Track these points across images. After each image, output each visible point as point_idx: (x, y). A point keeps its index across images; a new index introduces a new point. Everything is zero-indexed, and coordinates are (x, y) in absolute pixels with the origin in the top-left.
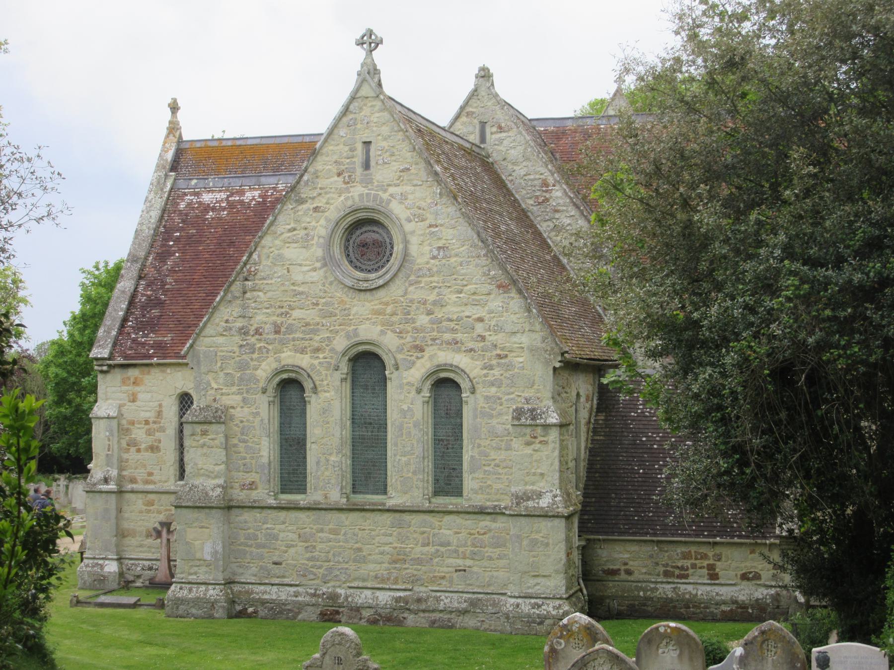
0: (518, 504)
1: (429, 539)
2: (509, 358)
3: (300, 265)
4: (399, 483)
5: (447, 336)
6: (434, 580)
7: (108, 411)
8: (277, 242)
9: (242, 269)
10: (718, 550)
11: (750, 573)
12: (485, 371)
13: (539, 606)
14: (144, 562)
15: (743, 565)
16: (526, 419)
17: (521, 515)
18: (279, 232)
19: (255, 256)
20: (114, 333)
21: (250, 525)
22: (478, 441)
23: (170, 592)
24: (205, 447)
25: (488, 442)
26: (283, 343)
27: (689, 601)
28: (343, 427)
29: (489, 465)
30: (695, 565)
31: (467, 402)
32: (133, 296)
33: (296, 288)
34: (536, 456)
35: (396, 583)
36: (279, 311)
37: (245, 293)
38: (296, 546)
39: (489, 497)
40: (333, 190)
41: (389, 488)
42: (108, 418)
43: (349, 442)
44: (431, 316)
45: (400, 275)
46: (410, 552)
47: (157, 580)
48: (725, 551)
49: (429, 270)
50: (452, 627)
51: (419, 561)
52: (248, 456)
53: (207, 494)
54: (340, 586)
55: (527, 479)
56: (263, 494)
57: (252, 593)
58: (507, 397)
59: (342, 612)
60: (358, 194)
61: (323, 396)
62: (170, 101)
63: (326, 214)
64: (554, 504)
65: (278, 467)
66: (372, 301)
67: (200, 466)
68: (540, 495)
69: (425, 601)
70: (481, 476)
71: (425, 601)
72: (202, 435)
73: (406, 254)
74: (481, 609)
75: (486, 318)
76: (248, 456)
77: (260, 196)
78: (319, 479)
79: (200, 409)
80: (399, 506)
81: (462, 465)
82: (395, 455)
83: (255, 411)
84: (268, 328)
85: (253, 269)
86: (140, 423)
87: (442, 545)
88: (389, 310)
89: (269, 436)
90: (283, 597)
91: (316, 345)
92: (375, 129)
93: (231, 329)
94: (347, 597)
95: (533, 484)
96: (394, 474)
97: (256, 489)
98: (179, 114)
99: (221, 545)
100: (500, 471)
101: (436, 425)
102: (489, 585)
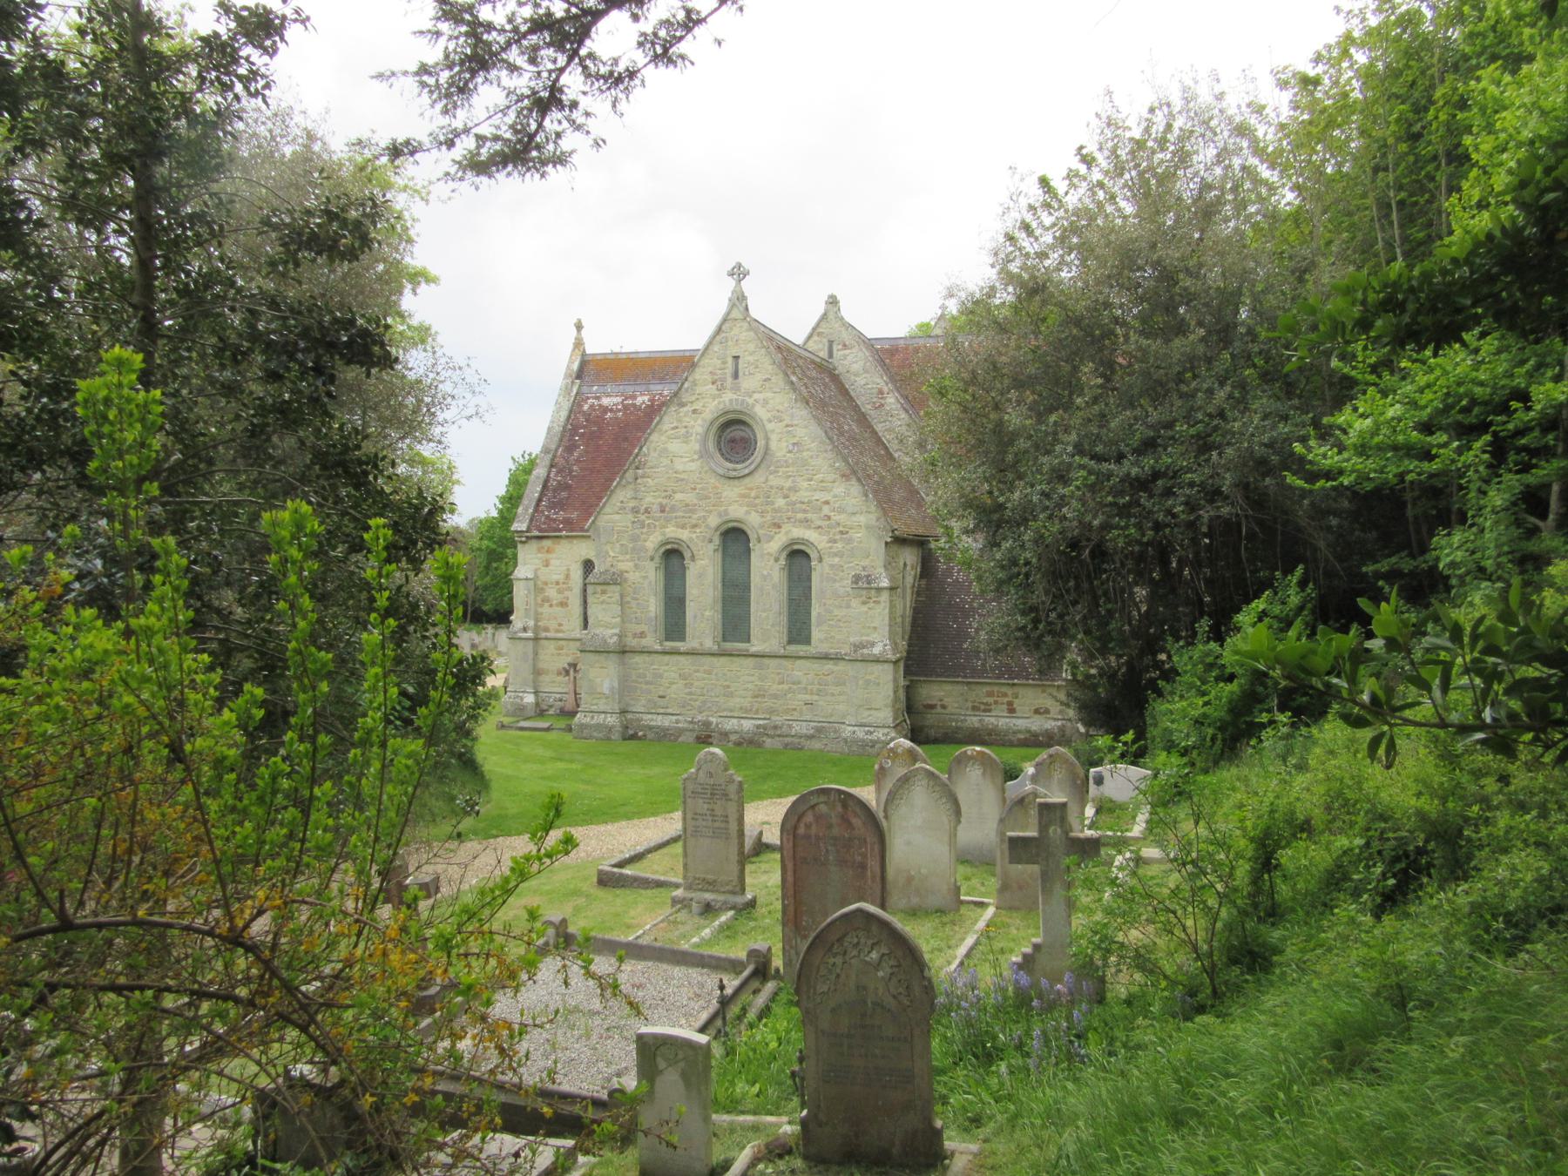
5: (800, 516)
6: (787, 711)
10: (1016, 689)
26: (668, 520)
28: (715, 588)
48: (1021, 691)
51: (775, 696)
56: (651, 641)
60: (728, 399)
68: (873, 644)
73: (767, 448)
84: (655, 508)
88: (753, 494)
101: (790, 588)
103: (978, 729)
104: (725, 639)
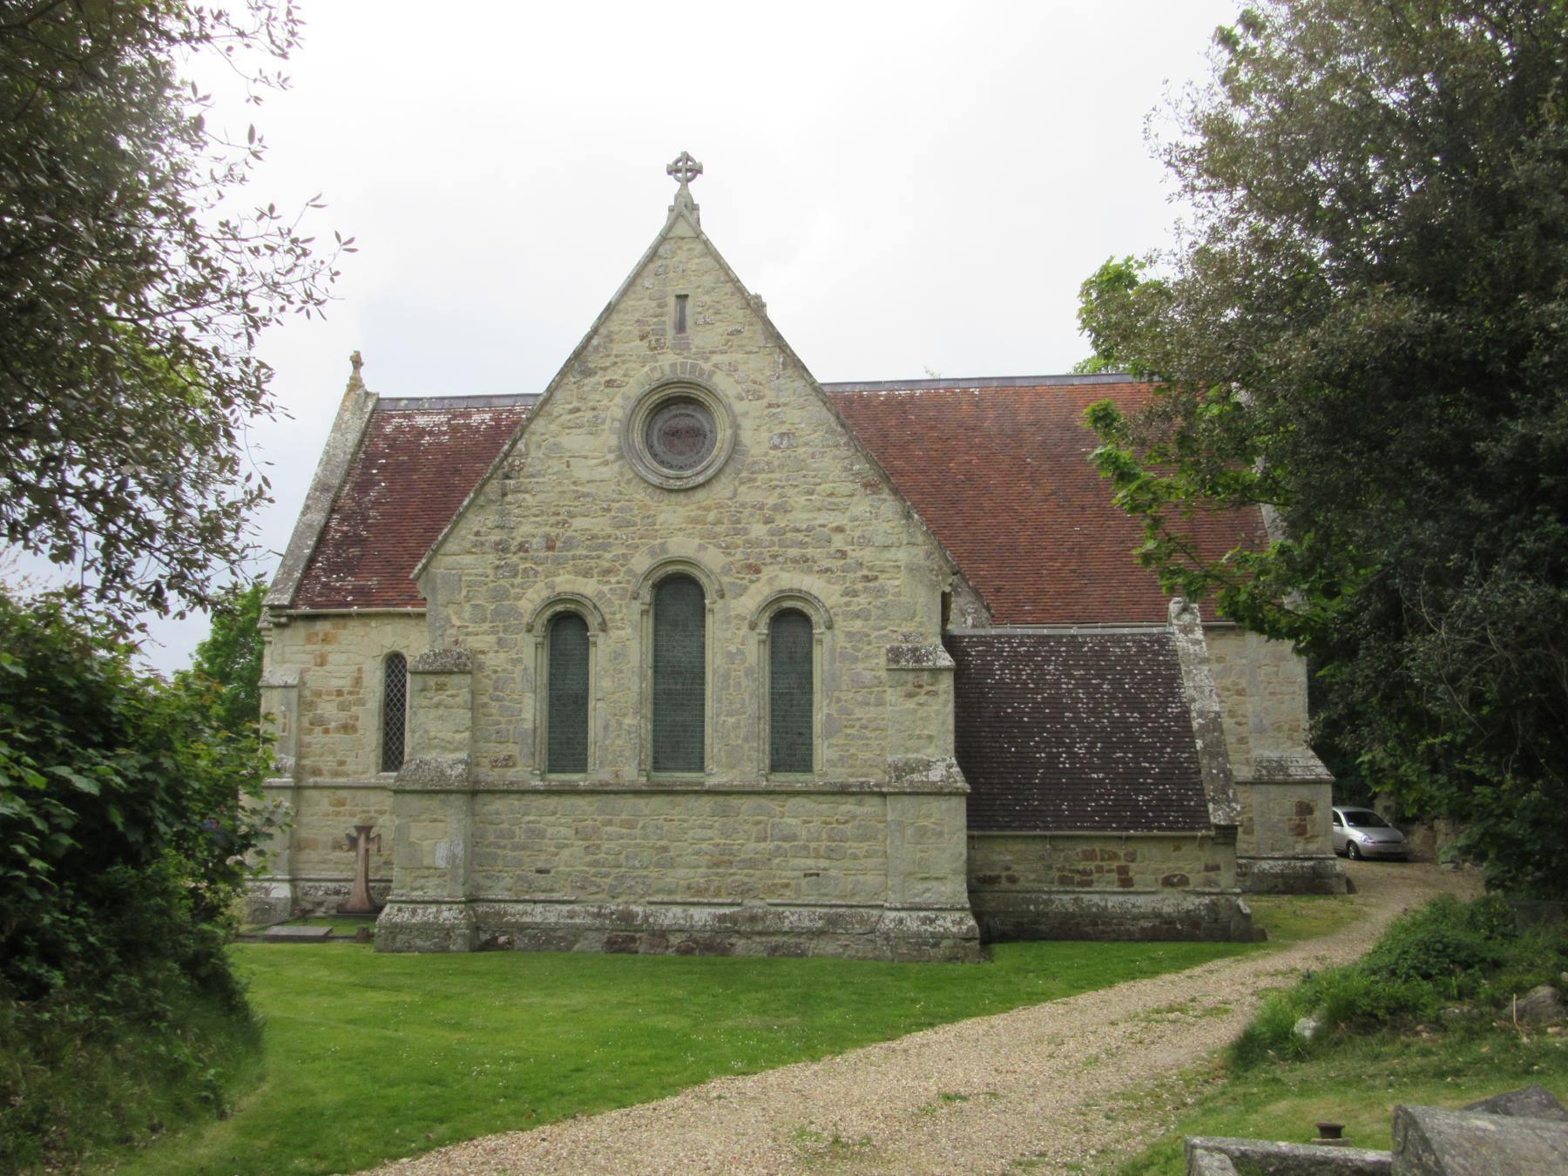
0: (898, 778)
1: (766, 832)
2: (880, 581)
3: (586, 457)
4: (723, 753)
5: (794, 552)
6: (771, 890)
7: (285, 678)
8: (553, 427)
9: (502, 462)
10: (1131, 847)
11: (1175, 876)
12: (846, 599)
13: (932, 921)
14: (329, 884)
15: (1164, 866)
16: (908, 661)
17: (905, 794)
18: (555, 414)
19: (520, 445)
20: (297, 575)
21: (503, 817)
22: (836, 694)
23: (382, 916)
24: (442, 708)
25: (851, 695)
26: (558, 562)
27: (1097, 916)
28: (642, 678)
29: (853, 727)
30: (1102, 867)
31: (820, 642)
32: (325, 529)
33: (579, 488)
34: (921, 713)
35: (717, 895)
36: (553, 520)
37: (504, 495)
38: (572, 845)
39: (852, 770)
40: (634, 358)
41: (707, 762)
42: (286, 687)
43: (650, 698)
44: (769, 526)
45: (728, 470)
46: (739, 850)
47: (349, 906)
48: (1143, 849)
49: (768, 463)
50: (803, 954)
51: (751, 863)
52: (503, 720)
53: (442, 773)
54: (635, 902)
55: (909, 743)
56: (525, 772)
57: (506, 914)
58: (876, 633)
59: (640, 938)
60: (668, 363)
61: (614, 634)
62: (352, 354)
63: (622, 390)
64: (949, 777)
65: (546, 735)
66: (686, 505)
67: (432, 734)
68: (928, 766)
69: (762, 919)
70: (841, 742)
71: (762, 919)
72: (437, 690)
73: (736, 443)
74: (845, 929)
75: (847, 528)
76: (503, 720)
77: (491, 419)
78: (607, 750)
79: (435, 654)
80: (724, 785)
81: (811, 728)
82: (718, 715)
83: (515, 656)
84: (537, 542)
85: (517, 463)
86: (329, 694)
87: (785, 839)
88: (711, 516)
89: (535, 692)
90: (553, 920)
91: (606, 565)
92: (693, 278)
93: (482, 544)
94: (646, 917)
95: (917, 750)
96: (716, 741)
97: (514, 765)
98: (363, 370)
99: (462, 846)
100: (869, 734)
101: (774, 675)
102: (853, 895)
103: (1073, 915)
104: (657, 766)
